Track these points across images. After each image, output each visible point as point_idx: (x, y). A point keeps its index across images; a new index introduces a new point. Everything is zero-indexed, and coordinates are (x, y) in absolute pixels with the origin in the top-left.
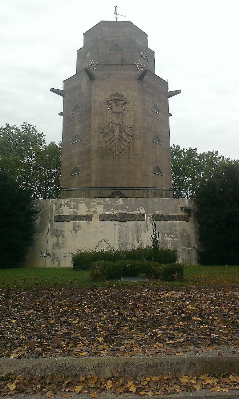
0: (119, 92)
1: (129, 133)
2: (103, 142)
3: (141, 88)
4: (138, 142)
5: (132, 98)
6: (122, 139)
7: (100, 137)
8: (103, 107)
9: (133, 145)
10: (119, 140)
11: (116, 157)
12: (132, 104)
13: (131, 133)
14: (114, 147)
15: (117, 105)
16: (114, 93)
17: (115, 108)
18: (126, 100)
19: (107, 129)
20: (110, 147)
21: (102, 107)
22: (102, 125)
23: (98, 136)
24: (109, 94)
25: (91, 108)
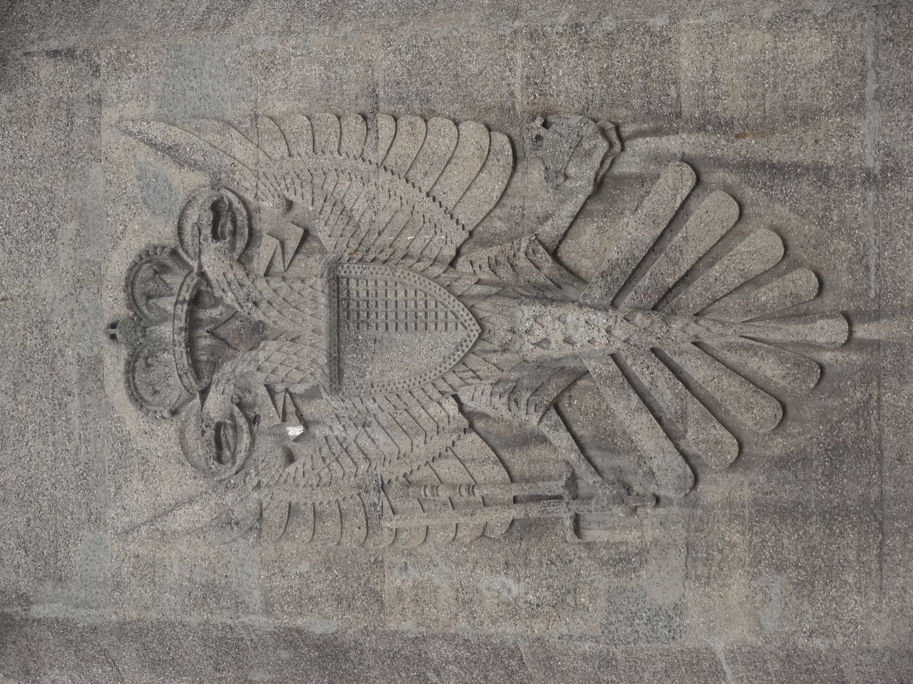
0: (114, 304)
1: (582, 177)
2: (690, 500)
3: (54, 44)
4: (688, 61)
5: (171, 151)
6: (660, 264)
7: (633, 536)
8: (283, 497)
9: (724, 126)
10: (663, 303)
11: (876, 345)
12: (241, 150)
13: (577, 150)
14: (753, 364)
15: (257, 332)
16: (114, 360)
17: (292, 357)
18: (193, 216)
19: (537, 452)
20: (756, 415)
21: (274, 516)
22: (481, 517)
23: (624, 561)
24: (131, 418)
25: (292, 638)
